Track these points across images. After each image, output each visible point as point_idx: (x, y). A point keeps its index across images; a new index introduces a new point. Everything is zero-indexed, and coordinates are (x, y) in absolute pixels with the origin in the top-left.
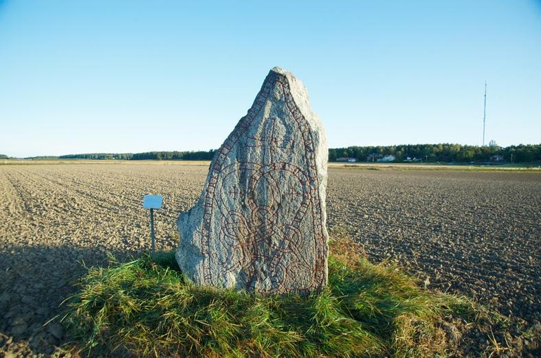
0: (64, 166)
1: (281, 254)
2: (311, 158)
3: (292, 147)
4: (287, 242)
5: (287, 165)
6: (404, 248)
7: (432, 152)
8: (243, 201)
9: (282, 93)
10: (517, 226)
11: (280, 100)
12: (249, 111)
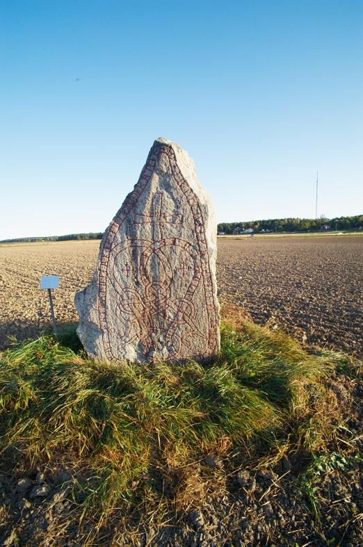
0: (3, 249)
1: (176, 325)
2: (201, 232)
3: (182, 221)
4: (181, 314)
5: (177, 241)
6: (277, 304)
7: (280, 225)
8: (136, 278)
9: (168, 165)
10: (359, 280)
11: (167, 173)
12: (136, 186)
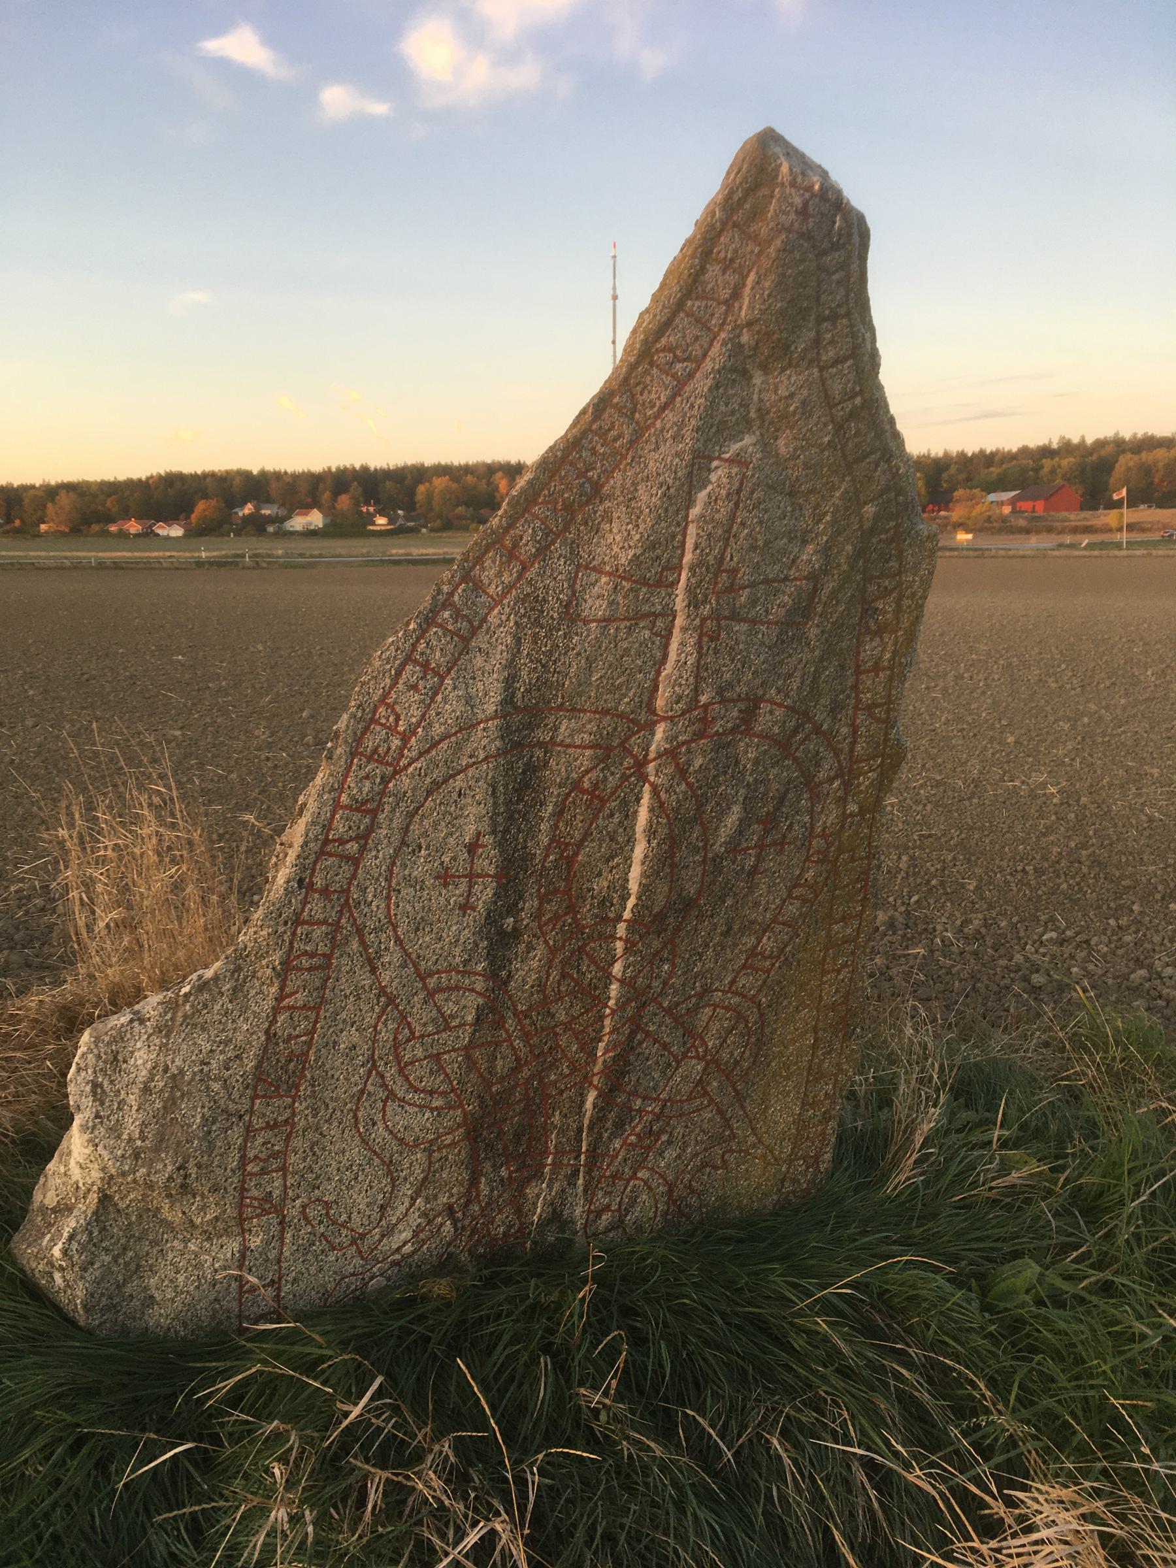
8: (512, 909)
